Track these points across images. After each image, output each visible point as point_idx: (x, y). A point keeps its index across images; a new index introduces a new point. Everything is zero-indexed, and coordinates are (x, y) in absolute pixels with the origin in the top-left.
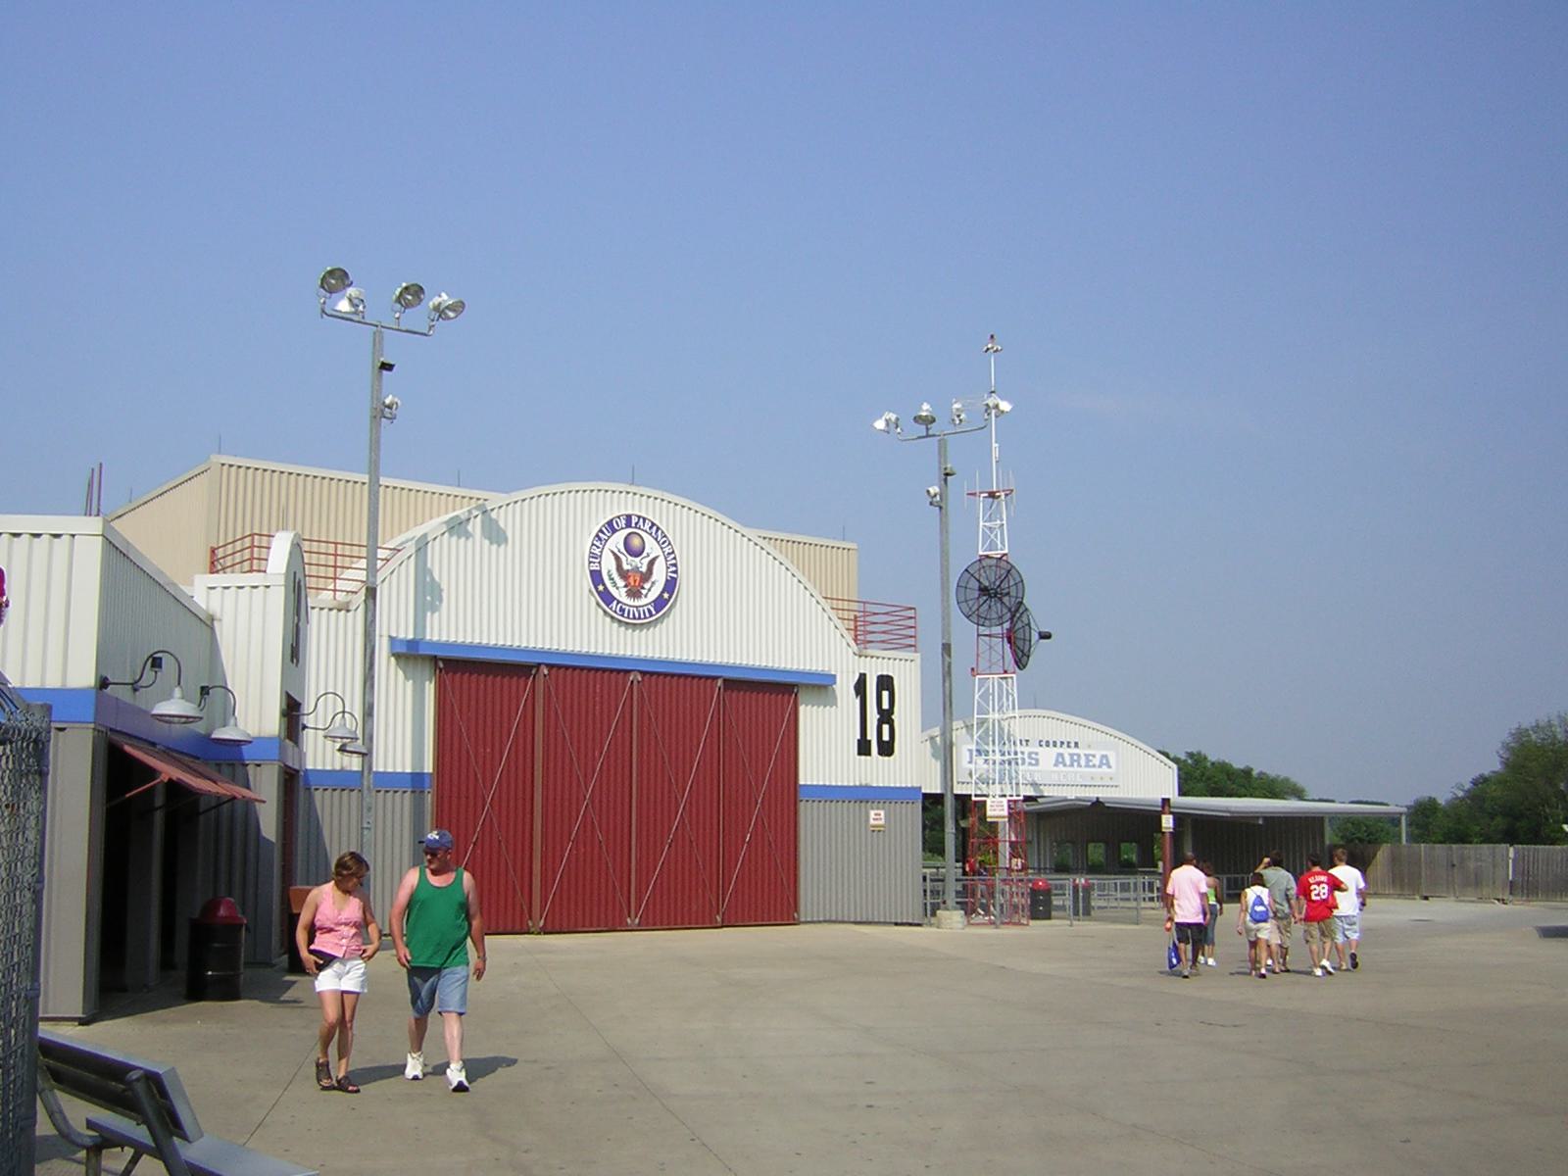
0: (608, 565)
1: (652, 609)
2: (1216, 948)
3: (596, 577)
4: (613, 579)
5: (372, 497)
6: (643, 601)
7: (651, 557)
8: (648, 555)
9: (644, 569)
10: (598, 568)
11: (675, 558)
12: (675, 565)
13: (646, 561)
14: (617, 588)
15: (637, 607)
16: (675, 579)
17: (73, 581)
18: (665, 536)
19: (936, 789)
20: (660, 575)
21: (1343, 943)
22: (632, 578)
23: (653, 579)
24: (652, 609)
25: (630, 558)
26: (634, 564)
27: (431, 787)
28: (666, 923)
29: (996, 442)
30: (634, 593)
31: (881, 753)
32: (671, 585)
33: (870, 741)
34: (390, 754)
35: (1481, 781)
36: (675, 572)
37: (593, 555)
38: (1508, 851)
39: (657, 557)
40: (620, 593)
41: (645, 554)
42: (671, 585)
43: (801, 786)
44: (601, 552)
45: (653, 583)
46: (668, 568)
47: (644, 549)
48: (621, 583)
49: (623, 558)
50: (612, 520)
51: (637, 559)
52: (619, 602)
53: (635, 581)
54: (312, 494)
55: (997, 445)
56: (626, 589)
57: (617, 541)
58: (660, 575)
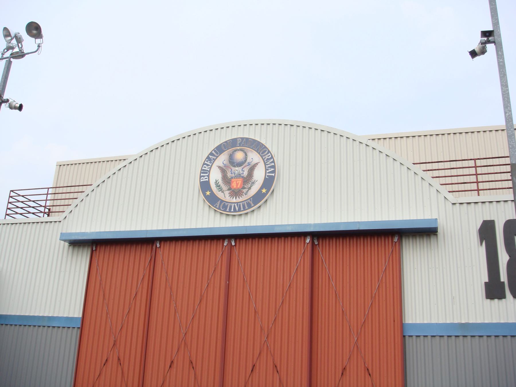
0: (215, 176)
1: (251, 203)
2: (495, 37)
3: (205, 186)
4: (219, 186)
9: (245, 173)
10: (207, 180)
11: (273, 162)
12: (274, 167)
14: (223, 192)
15: (237, 203)
16: (273, 177)
20: (259, 175)
22: (235, 183)
24: (251, 203)
26: (236, 172)
29: (503, 283)
34: (128, 345)
35: (88, 232)
36: (274, 172)
37: (203, 171)
39: (257, 164)
41: (246, 164)
43: (511, 162)
44: (210, 168)
45: (253, 183)
46: (266, 170)
47: (246, 161)
48: (224, 187)
54: (65, 175)
55: (502, 280)
56: (229, 191)
57: (222, 159)
58: (259, 175)
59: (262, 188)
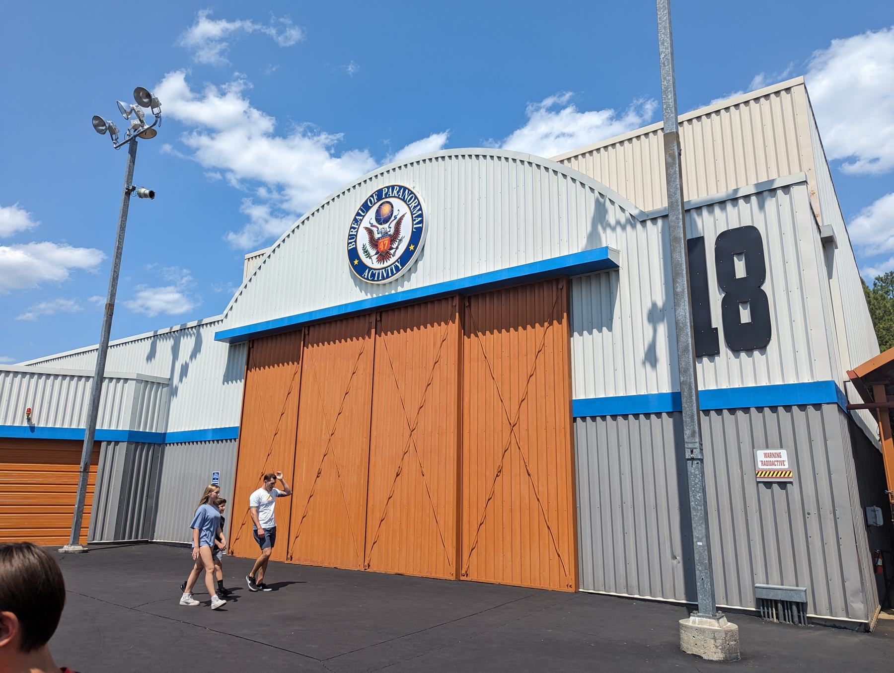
0: (363, 239)
1: (399, 265)
3: (353, 254)
5: (132, 171)
6: (393, 260)
7: (398, 217)
8: (395, 218)
12: (421, 215)
13: (393, 225)
14: (370, 258)
15: (385, 268)
16: (421, 228)
17: (737, 548)
18: (412, 193)
19: (669, 391)
21: (878, 558)
23: (401, 236)
24: (399, 265)
25: (380, 227)
27: (700, 622)
28: (105, 539)
30: (383, 256)
31: (736, 348)
32: (416, 236)
33: (716, 329)
38: (857, 627)
40: (372, 262)
41: (393, 218)
42: (416, 236)
45: (401, 240)
48: (372, 252)
49: (375, 229)
50: (366, 201)
51: (386, 226)
52: (370, 269)
53: (384, 245)
58: (406, 232)
59: (409, 245)
